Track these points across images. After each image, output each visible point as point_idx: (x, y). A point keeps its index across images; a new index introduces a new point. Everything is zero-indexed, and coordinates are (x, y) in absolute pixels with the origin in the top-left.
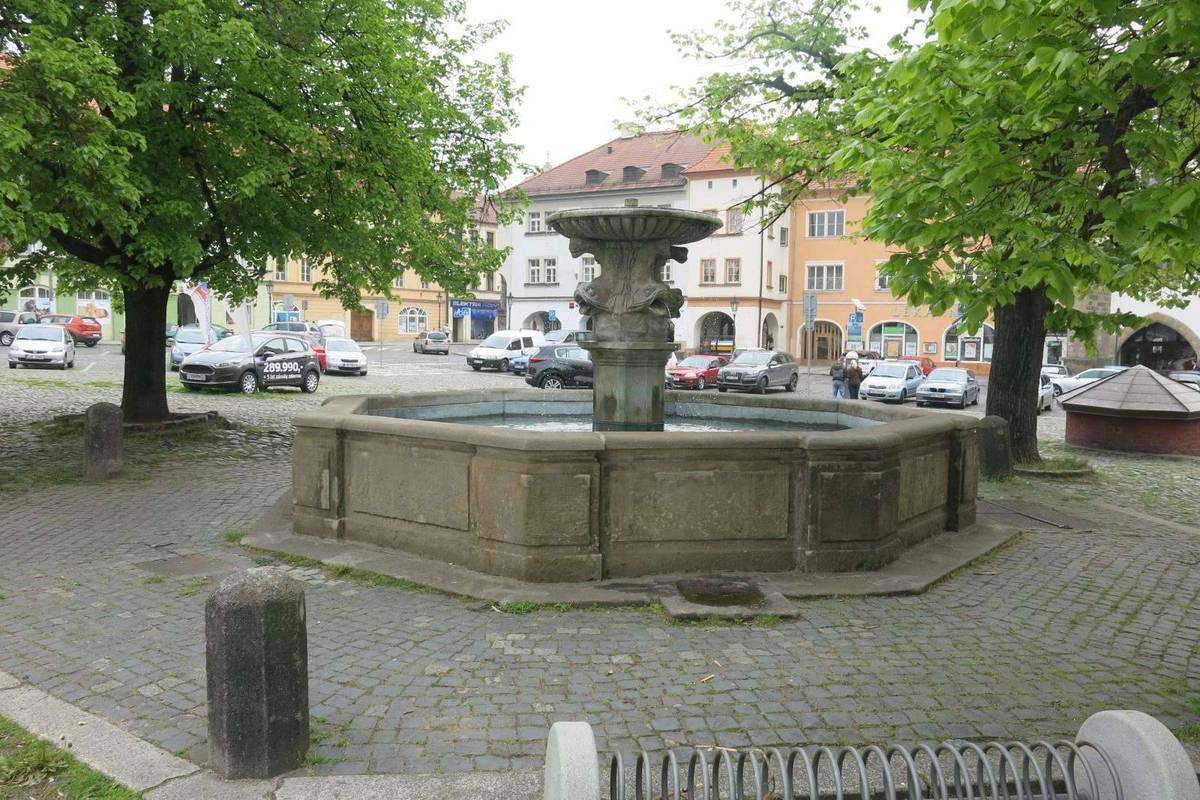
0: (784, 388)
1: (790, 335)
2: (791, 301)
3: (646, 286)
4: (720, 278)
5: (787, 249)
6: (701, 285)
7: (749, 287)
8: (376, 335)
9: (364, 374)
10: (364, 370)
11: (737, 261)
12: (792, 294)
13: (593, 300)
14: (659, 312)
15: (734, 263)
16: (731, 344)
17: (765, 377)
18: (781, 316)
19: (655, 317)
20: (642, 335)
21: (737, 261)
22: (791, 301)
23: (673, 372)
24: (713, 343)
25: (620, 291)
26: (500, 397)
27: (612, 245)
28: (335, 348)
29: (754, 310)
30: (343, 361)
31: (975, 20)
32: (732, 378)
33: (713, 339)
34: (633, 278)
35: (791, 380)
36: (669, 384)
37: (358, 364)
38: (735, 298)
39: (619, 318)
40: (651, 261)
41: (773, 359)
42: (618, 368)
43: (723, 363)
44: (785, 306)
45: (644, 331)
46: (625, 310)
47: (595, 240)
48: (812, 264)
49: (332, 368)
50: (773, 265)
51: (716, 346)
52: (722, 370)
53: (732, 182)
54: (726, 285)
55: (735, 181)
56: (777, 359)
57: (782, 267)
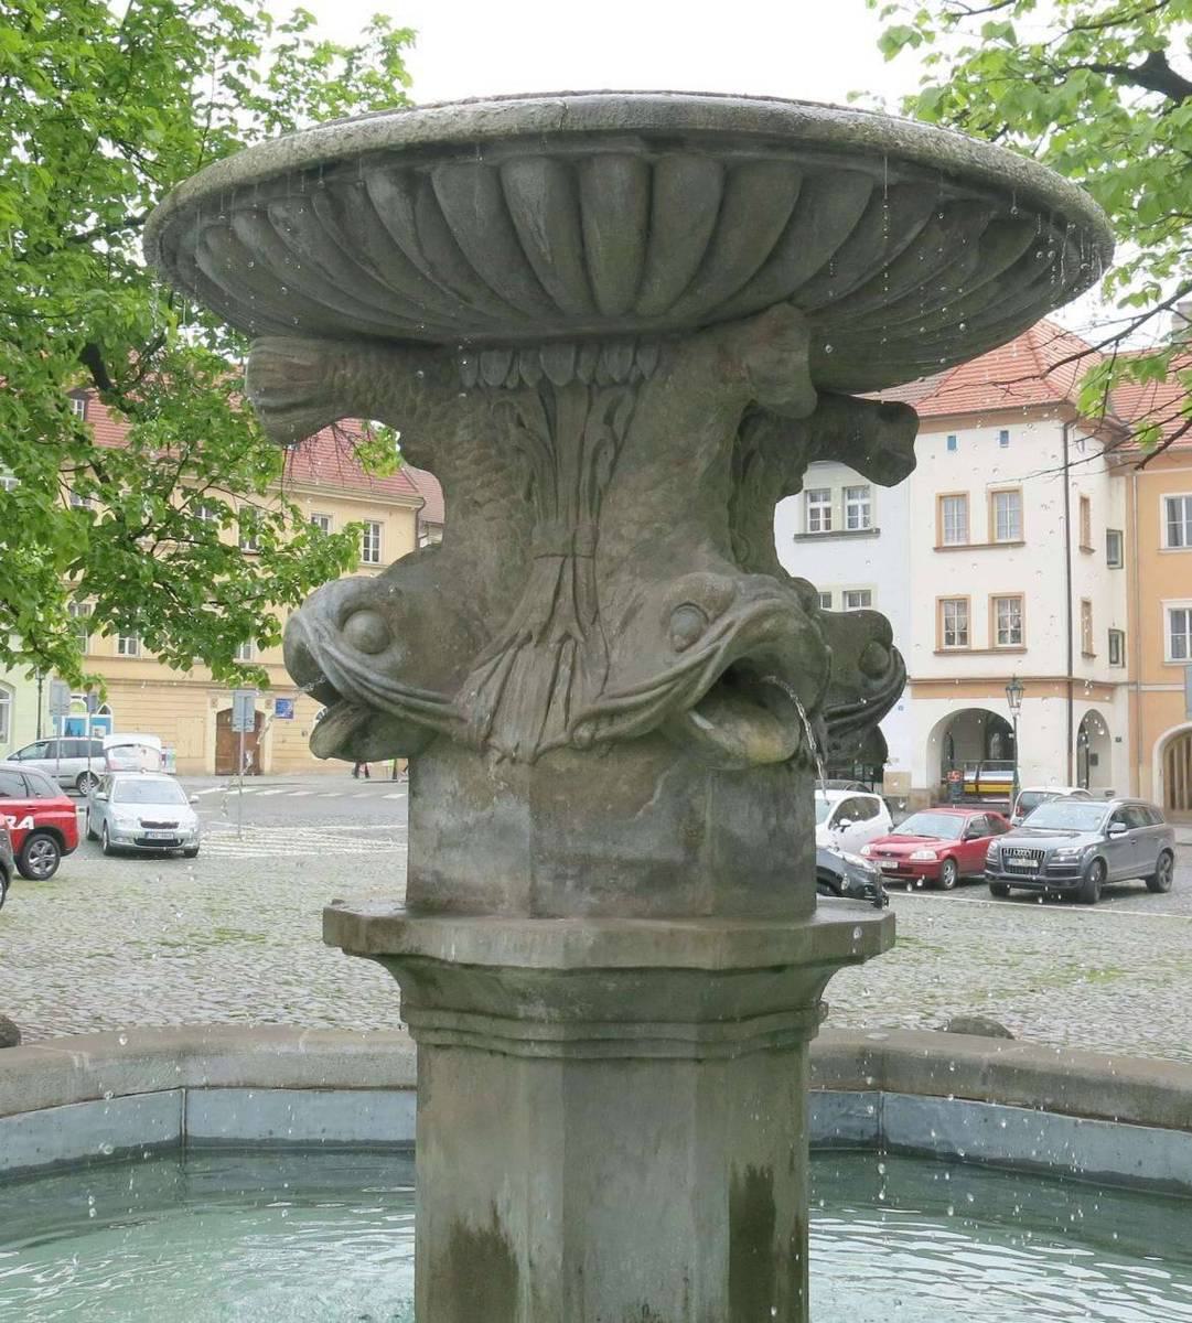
0: (1143, 883)
1: (1138, 758)
2: (1135, 683)
3: (677, 588)
4: (980, 636)
5: (1122, 574)
6: (939, 653)
7: (1044, 654)
8: (267, 763)
9: (191, 853)
10: (190, 845)
11: (1016, 601)
12: (1137, 669)
13: (375, 673)
14: (755, 740)
15: (1008, 605)
16: (1011, 778)
17: (1100, 860)
18: (1117, 716)
19: (737, 774)
20: (660, 877)
21: (1016, 601)
22: (1135, 683)
23: (882, 848)
24: (970, 777)
25: (537, 618)
26: (159, 1074)
27: (495, 370)
28: (135, 795)
29: (1057, 704)
30: (145, 825)
31: (773, 821)
32: (1022, 862)
33: (970, 768)
34: (610, 547)
35: (1159, 867)
36: (871, 888)
37: (180, 832)
38: (1014, 679)
39: (522, 773)
40: (710, 444)
41: (1114, 818)
42: (522, 1068)
43: (998, 826)
44: (1123, 695)
45: (678, 855)
46: (556, 731)
47: (397, 346)
48: (1178, 604)
49: (120, 842)
50: (1093, 606)
51: (977, 783)
52: (997, 843)
53: (997, 434)
54: (993, 651)
55: (1004, 434)
56: (1122, 816)
57: (1112, 612)
